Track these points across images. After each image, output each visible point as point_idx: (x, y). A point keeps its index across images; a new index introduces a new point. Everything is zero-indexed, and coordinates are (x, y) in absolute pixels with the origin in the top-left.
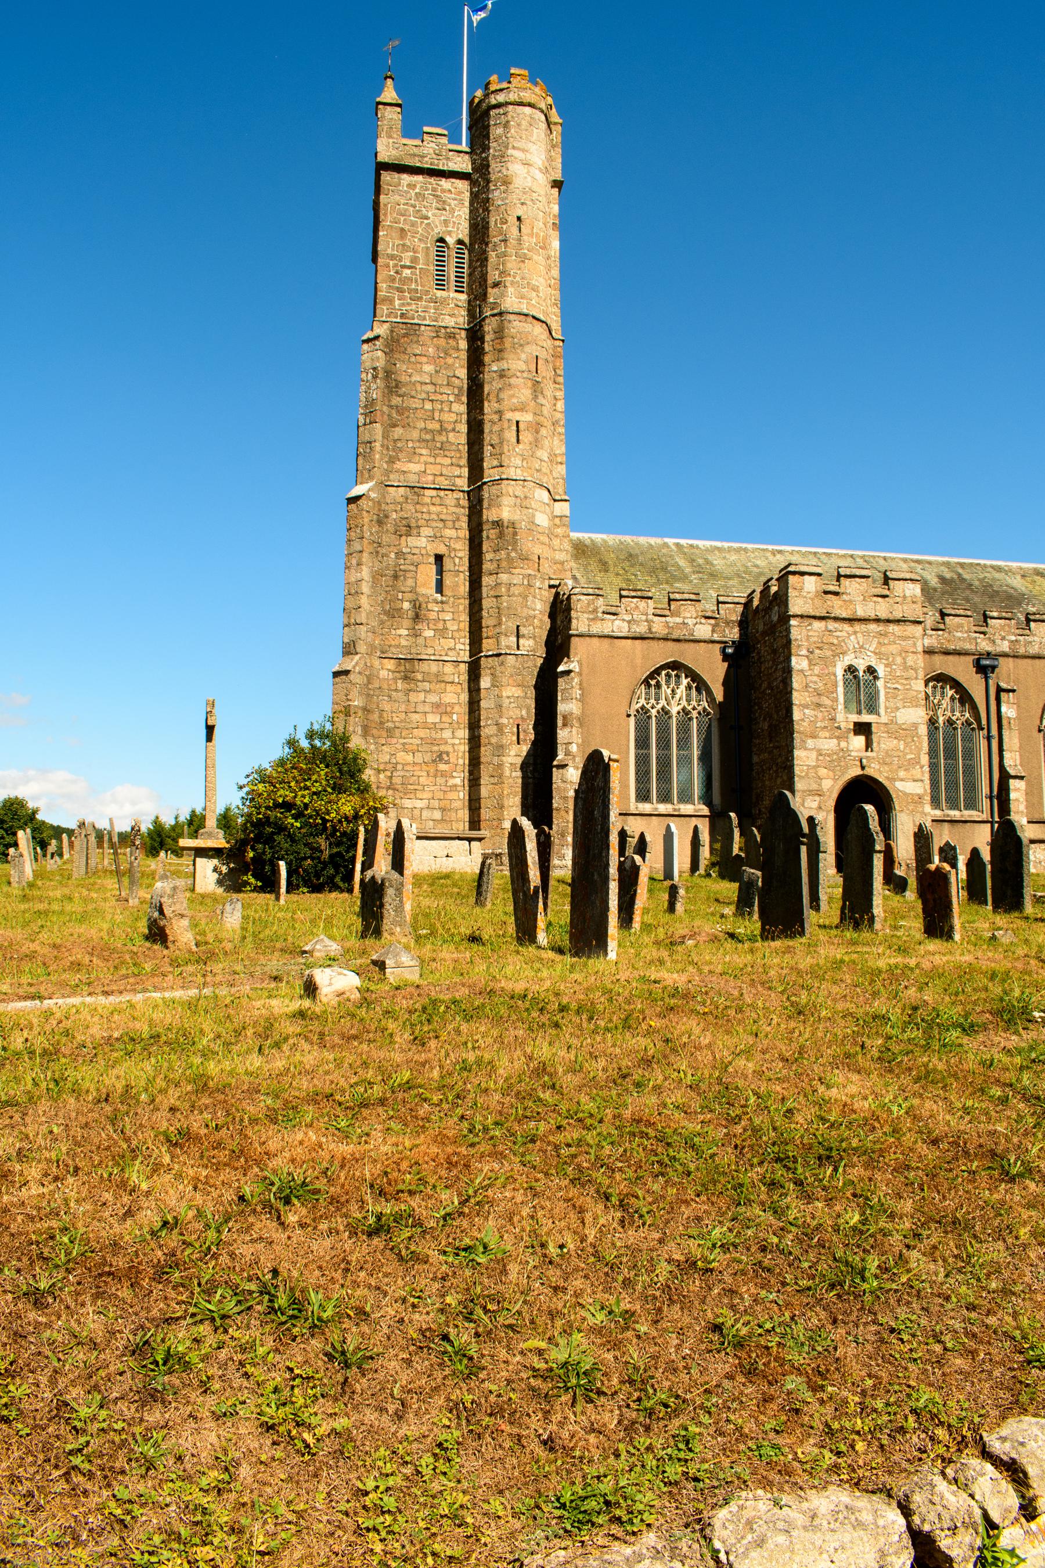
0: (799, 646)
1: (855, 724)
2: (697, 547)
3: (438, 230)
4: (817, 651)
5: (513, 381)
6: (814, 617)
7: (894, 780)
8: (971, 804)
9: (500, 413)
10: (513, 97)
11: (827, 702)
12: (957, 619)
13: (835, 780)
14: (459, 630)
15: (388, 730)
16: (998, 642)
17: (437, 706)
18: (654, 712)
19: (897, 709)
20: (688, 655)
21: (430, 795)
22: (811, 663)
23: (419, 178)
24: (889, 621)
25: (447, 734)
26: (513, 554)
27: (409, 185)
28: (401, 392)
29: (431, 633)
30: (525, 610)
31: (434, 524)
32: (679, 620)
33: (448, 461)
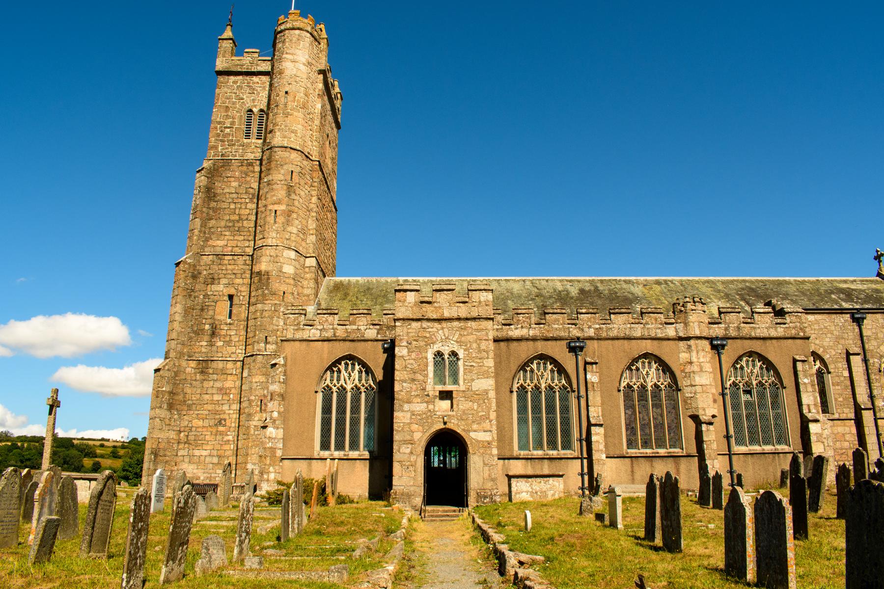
0: (401, 340)
1: (440, 392)
2: (419, 281)
3: (249, 105)
4: (414, 343)
5: (274, 187)
6: (413, 320)
7: (469, 431)
8: (567, 445)
9: (265, 206)
10: (288, 25)
11: (420, 377)
12: (554, 316)
13: (424, 433)
14: (239, 341)
15: (189, 406)
16: (586, 329)
17: (220, 389)
18: (529, 388)
19: (473, 380)
20: (359, 350)
21: (211, 447)
22: (410, 352)
23: (241, 77)
24: (467, 319)
25: (226, 407)
26: (266, 292)
27: (234, 82)
28: (216, 199)
29: (221, 344)
30: (271, 326)
31: (229, 276)
32: (355, 327)
33: (242, 238)
